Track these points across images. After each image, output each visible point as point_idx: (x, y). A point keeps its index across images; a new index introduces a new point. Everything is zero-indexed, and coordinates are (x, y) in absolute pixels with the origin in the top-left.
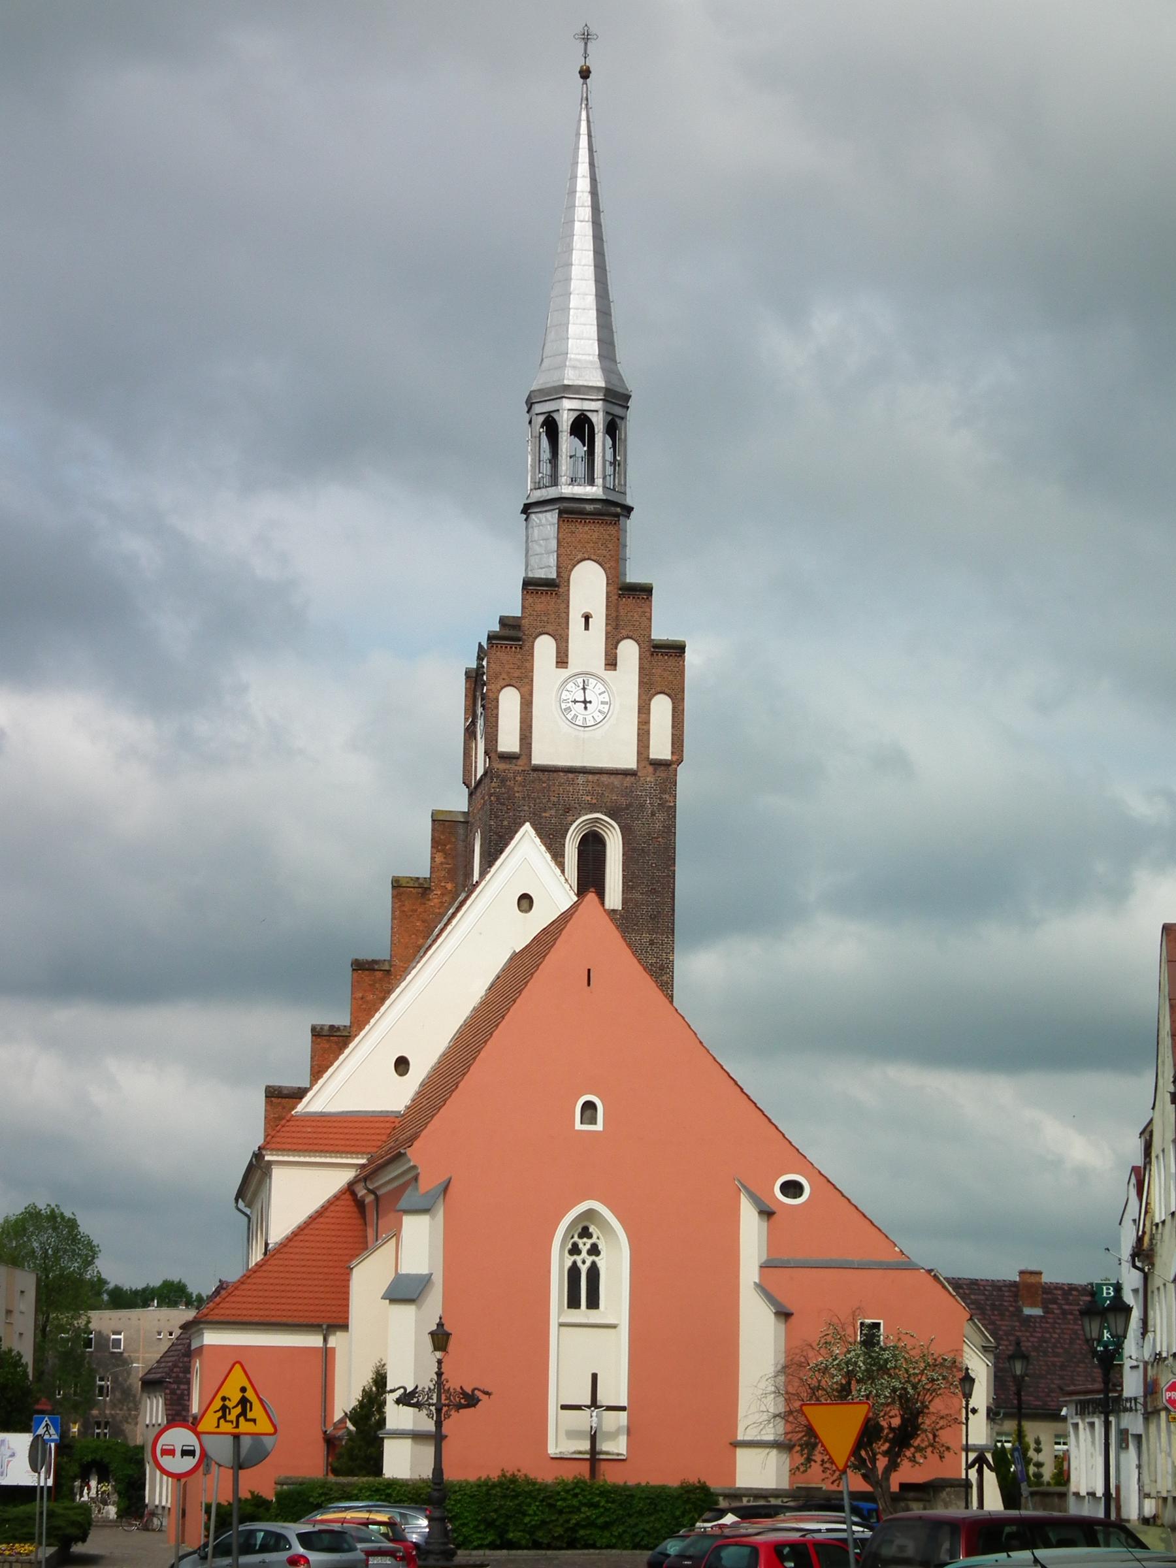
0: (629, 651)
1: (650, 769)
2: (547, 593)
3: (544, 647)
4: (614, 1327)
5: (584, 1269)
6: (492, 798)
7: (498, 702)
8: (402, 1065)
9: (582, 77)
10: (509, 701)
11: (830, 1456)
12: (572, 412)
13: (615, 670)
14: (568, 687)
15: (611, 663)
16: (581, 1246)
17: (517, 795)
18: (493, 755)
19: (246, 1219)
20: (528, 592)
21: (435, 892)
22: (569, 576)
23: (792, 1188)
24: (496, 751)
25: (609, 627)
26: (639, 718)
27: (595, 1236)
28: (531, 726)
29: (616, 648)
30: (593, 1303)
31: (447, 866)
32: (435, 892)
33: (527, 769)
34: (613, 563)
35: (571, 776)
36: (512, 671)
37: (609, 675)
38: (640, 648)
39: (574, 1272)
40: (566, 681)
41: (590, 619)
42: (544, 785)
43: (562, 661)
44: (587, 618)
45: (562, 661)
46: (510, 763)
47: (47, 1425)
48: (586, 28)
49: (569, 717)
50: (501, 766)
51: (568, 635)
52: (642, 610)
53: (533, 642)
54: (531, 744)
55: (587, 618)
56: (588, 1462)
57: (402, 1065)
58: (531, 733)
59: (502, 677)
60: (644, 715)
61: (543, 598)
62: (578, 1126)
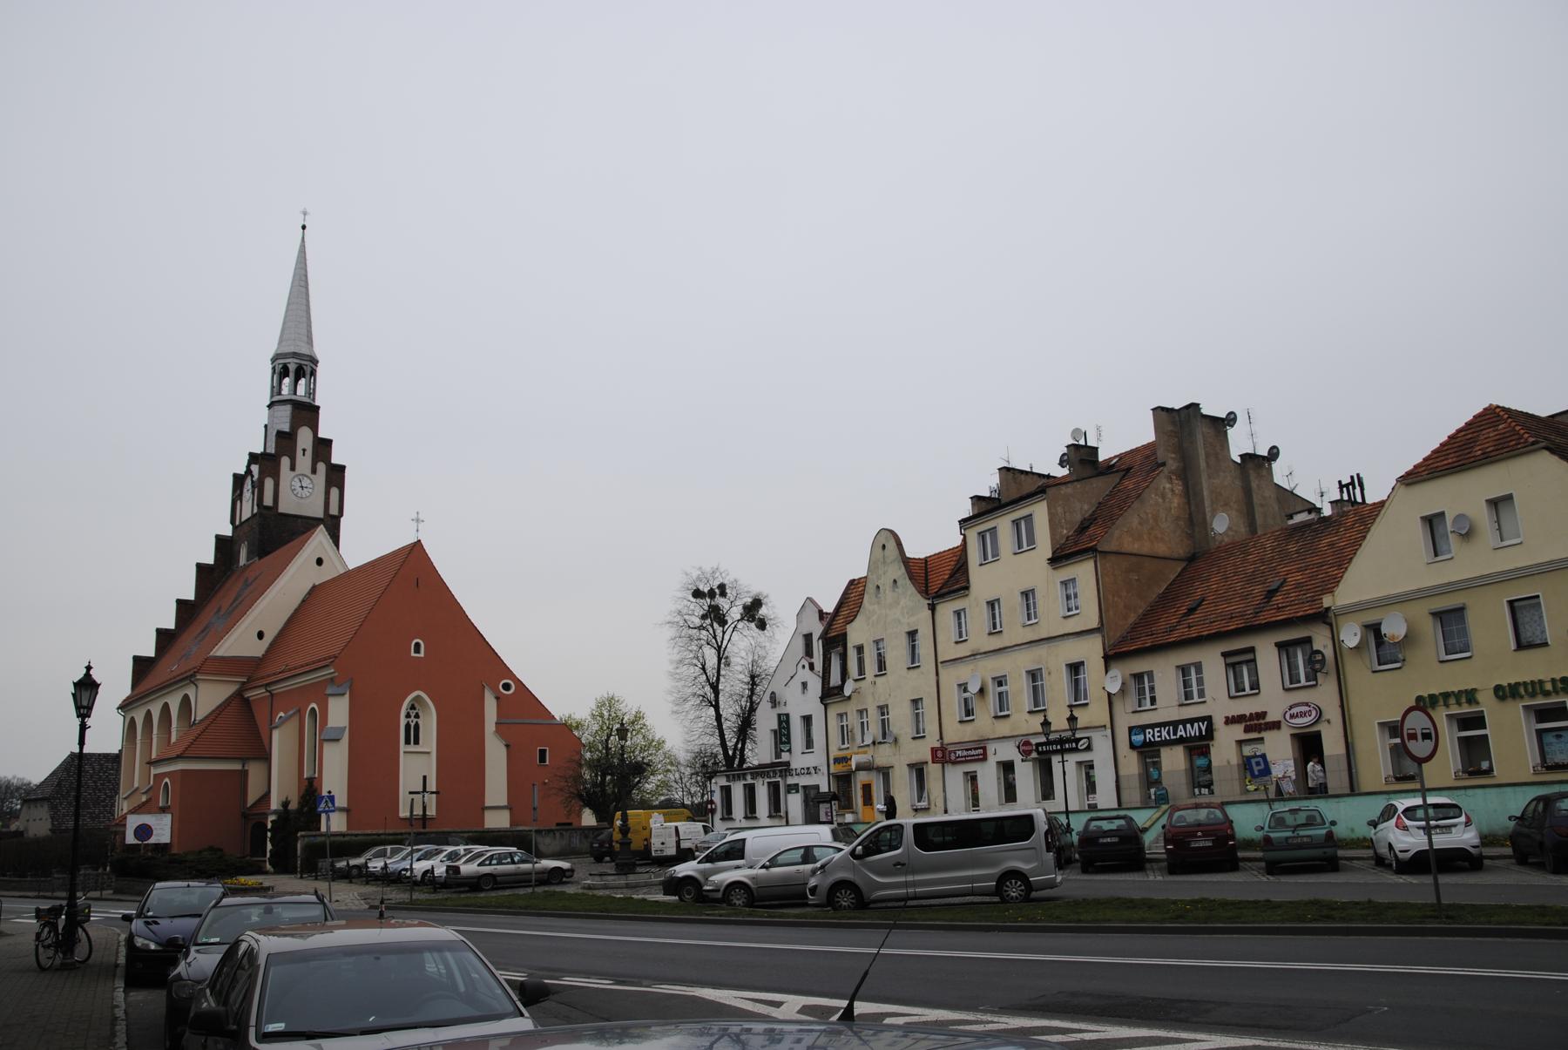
0: (321, 467)
1: (329, 519)
3: (285, 461)
4: (428, 753)
5: (412, 725)
8: (261, 635)
10: (269, 484)
11: (1193, 664)
15: (314, 471)
23: (507, 687)
30: (417, 742)
34: (315, 429)
37: (312, 476)
39: (408, 726)
40: (294, 477)
43: (293, 468)
44: (304, 450)
45: (293, 468)
47: (326, 801)
50: (265, 512)
55: (304, 450)
56: (488, 804)
57: (261, 635)
62: (413, 654)
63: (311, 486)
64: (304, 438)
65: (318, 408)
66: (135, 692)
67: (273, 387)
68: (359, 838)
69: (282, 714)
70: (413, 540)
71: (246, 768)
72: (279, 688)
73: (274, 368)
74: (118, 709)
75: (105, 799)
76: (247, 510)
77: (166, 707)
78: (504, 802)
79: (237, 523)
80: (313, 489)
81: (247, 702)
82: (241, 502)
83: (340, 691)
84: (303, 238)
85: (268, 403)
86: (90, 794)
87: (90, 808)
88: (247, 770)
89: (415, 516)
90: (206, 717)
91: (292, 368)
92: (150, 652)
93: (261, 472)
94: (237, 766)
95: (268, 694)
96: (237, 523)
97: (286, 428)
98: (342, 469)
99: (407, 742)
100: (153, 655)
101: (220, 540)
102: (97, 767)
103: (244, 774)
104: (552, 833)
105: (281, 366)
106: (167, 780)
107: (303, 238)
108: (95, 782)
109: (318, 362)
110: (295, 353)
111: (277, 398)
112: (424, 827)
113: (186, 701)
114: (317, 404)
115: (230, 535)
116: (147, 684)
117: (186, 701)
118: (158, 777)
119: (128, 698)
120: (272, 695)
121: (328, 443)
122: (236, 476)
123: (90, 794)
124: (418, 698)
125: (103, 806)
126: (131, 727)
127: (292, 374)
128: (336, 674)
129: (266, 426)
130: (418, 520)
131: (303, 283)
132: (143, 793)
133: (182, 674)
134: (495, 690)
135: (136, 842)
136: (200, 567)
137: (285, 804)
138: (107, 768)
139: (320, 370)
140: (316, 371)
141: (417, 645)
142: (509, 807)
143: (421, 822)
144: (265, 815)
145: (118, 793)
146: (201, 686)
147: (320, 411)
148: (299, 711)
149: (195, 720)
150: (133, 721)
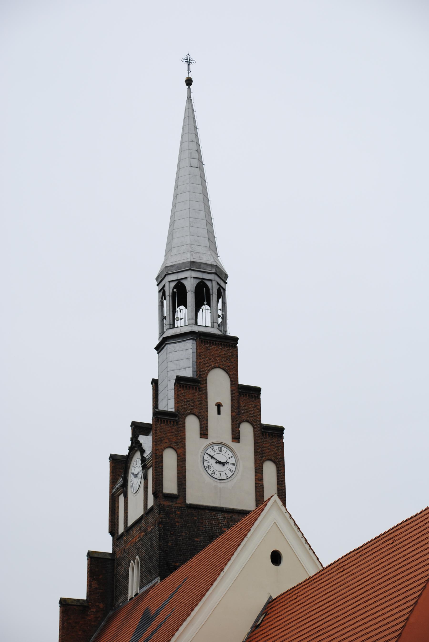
2: (193, 387)
6: (160, 526)
7: (162, 458)
9: (187, 85)
12: (195, 280)
13: (239, 442)
15: (236, 437)
17: (177, 524)
18: (160, 495)
20: (180, 386)
21: (92, 610)
22: (206, 377)
24: (162, 492)
25: (234, 413)
26: (255, 476)
29: (239, 428)
31: (100, 591)
32: (92, 610)
33: (183, 506)
35: (213, 513)
36: (171, 437)
37: (234, 445)
41: (221, 407)
42: (196, 518)
43: (204, 434)
44: (219, 406)
45: (204, 434)
46: (172, 501)
48: (188, 56)
49: (210, 472)
50: (166, 503)
51: (207, 416)
52: (254, 403)
53: (185, 419)
54: (185, 489)
55: (219, 406)
58: (185, 481)
59: (165, 441)
60: (259, 475)
61: (191, 391)
63: (232, 461)
65: (235, 339)
67: (162, 318)
73: (162, 292)
79: (121, 530)
80: (236, 465)
82: (126, 497)
84: (189, 97)
85: (157, 342)
93: (155, 443)
96: (121, 530)
97: (189, 373)
105: (173, 284)
107: (189, 97)
109: (226, 276)
110: (192, 263)
114: (231, 332)
122: (114, 459)
127: (190, 298)
129: (155, 382)
131: (195, 163)
136: (129, 447)
140: (224, 290)
147: (261, 392)
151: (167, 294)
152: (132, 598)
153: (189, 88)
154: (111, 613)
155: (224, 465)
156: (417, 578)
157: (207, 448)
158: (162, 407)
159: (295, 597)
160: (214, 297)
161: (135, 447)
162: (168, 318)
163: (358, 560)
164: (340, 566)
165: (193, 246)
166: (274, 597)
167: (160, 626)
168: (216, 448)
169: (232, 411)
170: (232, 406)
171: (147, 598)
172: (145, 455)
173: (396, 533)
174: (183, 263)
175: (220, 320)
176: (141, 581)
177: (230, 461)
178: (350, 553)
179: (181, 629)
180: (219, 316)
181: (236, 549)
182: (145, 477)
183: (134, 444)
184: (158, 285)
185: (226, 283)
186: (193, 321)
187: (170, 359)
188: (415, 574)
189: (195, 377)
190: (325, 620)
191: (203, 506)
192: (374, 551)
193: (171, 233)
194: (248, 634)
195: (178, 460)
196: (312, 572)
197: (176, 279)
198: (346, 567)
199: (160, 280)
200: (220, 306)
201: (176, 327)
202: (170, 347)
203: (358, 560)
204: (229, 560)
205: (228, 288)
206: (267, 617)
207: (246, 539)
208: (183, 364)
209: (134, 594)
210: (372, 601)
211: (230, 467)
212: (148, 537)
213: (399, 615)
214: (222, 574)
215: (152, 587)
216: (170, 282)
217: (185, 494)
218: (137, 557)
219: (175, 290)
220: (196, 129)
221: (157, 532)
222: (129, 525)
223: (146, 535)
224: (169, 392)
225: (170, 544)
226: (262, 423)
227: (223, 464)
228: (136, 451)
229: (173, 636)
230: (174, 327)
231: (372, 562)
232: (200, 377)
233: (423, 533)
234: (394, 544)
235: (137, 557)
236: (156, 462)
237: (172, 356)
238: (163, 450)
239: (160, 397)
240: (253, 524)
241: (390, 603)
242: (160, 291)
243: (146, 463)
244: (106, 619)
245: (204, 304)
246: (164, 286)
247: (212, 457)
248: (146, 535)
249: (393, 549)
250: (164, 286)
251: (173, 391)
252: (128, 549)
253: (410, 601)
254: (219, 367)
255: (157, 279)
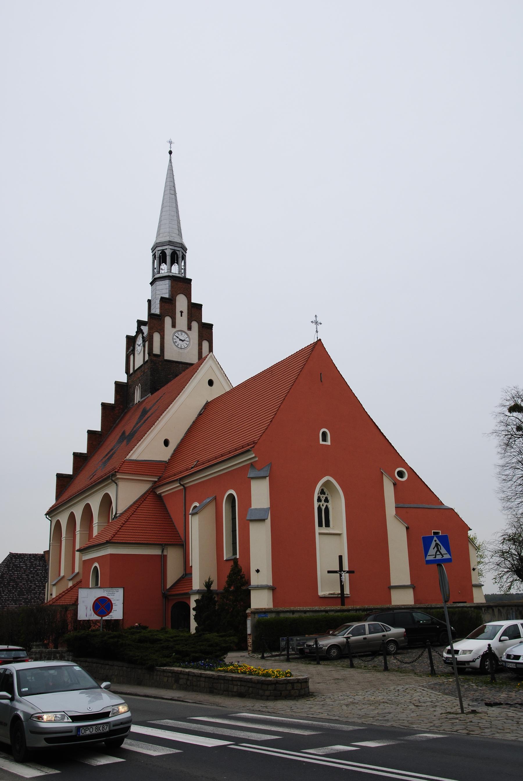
3: (168, 321)
4: (339, 535)
5: (323, 508)
7: (153, 337)
8: (166, 443)
9: (169, 154)
10: (156, 337)
13: (191, 330)
14: (179, 333)
15: (190, 328)
16: (321, 498)
18: (151, 354)
19: (50, 521)
26: (199, 347)
27: (326, 494)
28: (164, 346)
29: (191, 323)
30: (328, 525)
35: (177, 364)
37: (188, 332)
38: (198, 325)
39: (319, 509)
43: (174, 325)
44: (182, 312)
45: (174, 325)
47: (437, 545)
50: (155, 359)
53: (164, 318)
55: (182, 312)
57: (166, 443)
58: (164, 348)
62: (321, 442)
63: (187, 339)
64: (181, 303)
65: (191, 280)
66: (60, 501)
67: (154, 269)
68: (308, 615)
69: (197, 504)
70: (313, 340)
71: (165, 553)
72: (190, 482)
73: (154, 256)
74: (46, 515)
75: (35, 588)
76: (139, 360)
77: (88, 508)
78: (408, 583)
79: (131, 371)
81: (159, 498)
82: (134, 356)
83: (262, 474)
84: (170, 160)
86: (24, 584)
87: (24, 595)
88: (166, 556)
89: (314, 319)
90: (126, 511)
91: (168, 252)
92: (69, 470)
93: (150, 329)
94: (157, 552)
95: (182, 487)
96: (131, 371)
97: (167, 296)
98: (210, 326)
99: (320, 525)
100: (71, 473)
101: (118, 385)
102: (29, 564)
103: (163, 558)
104: (490, 611)
105: (160, 252)
106: (96, 564)
107: (170, 160)
108: (27, 575)
109: (187, 249)
110: (170, 241)
111: (157, 276)
112: (343, 604)
113: (107, 501)
114: (188, 276)
115: (126, 381)
116: (65, 496)
117: (107, 501)
118: (86, 564)
119: (53, 506)
120: (185, 488)
121: (199, 307)
122: (128, 337)
123: (24, 584)
124: (328, 482)
125: (34, 594)
126: (57, 529)
128: (257, 459)
129: (149, 301)
130: (316, 323)
131: (172, 192)
132: (70, 580)
133: (144, 422)
134: (392, 477)
135: (99, 618)
136: (105, 406)
137: (208, 584)
138: (35, 564)
139: (188, 255)
140: (185, 256)
141: (324, 434)
142: (413, 586)
143: (339, 601)
144: (188, 596)
145: (48, 581)
146: (121, 484)
148: (215, 498)
149: (116, 514)
150: (58, 524)
151: (157, 256)
152: (137, 403)
153: (170, 155)
154: (126, 411)
155: (183, 341)
156: (284, 388)
157: (175, 333)
158: (153, 312)
159: (220, 400)
160: (180, 259)
161: (139, 331)
162: (157, 268)
163: (254, 382)
164: (244, 385)
165: (170, 233)
166: (209, 401)
167: (152, 414)
168: (179, 333)
169: (188, 315)
170: (188, 313)
171: (144, 403)
172: (144, 335)
173: (273, 369)
174: (165, 241)
175: (183, 271)
176: (141, 396)
177: (186, 339)
178: (249, 379)
179: (164, 414)
180: (182, 269)
181: (191, 378)
182: (144, 346)
183: (139, 330)
184: (152, 252)
185: (186, 253)
186: (169, 271)
187: (157, 289)
188: (285, 385)
189: (170, 297)
190: (236, 410)
191: (172, 360)
192: (262, 377)
193: (159, 227)
194: (196, 418)
195: (161, 338)
196: (228, 389)
197: (161, 249)
198: (247, 385)
199: (153, 249)
200: (183, 264)
201: (161, 273)
202: (157, 283)
203: (254, 382)
204: (188, 383)
205: (188, 255)
206: (205, 410)
207: (196, 373)
208: (164, 291)
209: (138, 402)
210: (261, 400)
211: (186, 342)
212: (145, 375)
213: (275, 405)
214: (184, 389)
215: (147, 398)
216: (158, 250)
217: (164, 355)
218: (139, 384)
219: (161, 255)
220: (173, 176)
221: (150, 373)
222: (135, 369)
223: (144, 373)
224: (156, 305)
225: (156, 378)
226: (203, 322)
227: (183, 341)
228: (140, 333)
229: (159, 417)
230: (160, 273)
231: (245, 408)
232: (172, 298)
233: (287, 367)
234: (272, 374)
235: (139, 384)
236: (150, 338)
237: (158, 288)
238: (153, 333)
239: (152, 308)
240: (200, 366)
241: (270, 400)
242: (153, 255)
243: (145, 339)
244: (124, 413)
245: (175, 263)
246: (155, 252)
247: (178, 337)
248: (144, 373)
249: (272, 376)
250: (155, 252)
251: (159, 305)
252: (135, 381)
253: (261, 431)
254: (182, 293)
255: (152, 249)
